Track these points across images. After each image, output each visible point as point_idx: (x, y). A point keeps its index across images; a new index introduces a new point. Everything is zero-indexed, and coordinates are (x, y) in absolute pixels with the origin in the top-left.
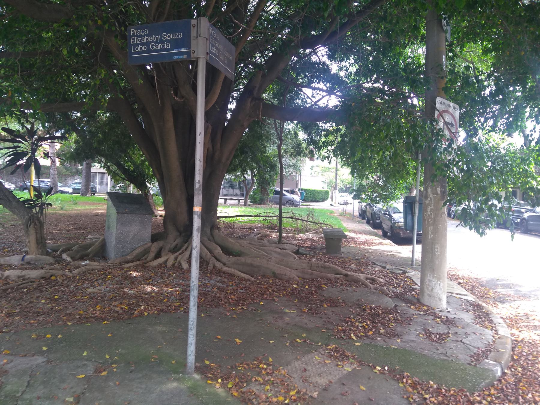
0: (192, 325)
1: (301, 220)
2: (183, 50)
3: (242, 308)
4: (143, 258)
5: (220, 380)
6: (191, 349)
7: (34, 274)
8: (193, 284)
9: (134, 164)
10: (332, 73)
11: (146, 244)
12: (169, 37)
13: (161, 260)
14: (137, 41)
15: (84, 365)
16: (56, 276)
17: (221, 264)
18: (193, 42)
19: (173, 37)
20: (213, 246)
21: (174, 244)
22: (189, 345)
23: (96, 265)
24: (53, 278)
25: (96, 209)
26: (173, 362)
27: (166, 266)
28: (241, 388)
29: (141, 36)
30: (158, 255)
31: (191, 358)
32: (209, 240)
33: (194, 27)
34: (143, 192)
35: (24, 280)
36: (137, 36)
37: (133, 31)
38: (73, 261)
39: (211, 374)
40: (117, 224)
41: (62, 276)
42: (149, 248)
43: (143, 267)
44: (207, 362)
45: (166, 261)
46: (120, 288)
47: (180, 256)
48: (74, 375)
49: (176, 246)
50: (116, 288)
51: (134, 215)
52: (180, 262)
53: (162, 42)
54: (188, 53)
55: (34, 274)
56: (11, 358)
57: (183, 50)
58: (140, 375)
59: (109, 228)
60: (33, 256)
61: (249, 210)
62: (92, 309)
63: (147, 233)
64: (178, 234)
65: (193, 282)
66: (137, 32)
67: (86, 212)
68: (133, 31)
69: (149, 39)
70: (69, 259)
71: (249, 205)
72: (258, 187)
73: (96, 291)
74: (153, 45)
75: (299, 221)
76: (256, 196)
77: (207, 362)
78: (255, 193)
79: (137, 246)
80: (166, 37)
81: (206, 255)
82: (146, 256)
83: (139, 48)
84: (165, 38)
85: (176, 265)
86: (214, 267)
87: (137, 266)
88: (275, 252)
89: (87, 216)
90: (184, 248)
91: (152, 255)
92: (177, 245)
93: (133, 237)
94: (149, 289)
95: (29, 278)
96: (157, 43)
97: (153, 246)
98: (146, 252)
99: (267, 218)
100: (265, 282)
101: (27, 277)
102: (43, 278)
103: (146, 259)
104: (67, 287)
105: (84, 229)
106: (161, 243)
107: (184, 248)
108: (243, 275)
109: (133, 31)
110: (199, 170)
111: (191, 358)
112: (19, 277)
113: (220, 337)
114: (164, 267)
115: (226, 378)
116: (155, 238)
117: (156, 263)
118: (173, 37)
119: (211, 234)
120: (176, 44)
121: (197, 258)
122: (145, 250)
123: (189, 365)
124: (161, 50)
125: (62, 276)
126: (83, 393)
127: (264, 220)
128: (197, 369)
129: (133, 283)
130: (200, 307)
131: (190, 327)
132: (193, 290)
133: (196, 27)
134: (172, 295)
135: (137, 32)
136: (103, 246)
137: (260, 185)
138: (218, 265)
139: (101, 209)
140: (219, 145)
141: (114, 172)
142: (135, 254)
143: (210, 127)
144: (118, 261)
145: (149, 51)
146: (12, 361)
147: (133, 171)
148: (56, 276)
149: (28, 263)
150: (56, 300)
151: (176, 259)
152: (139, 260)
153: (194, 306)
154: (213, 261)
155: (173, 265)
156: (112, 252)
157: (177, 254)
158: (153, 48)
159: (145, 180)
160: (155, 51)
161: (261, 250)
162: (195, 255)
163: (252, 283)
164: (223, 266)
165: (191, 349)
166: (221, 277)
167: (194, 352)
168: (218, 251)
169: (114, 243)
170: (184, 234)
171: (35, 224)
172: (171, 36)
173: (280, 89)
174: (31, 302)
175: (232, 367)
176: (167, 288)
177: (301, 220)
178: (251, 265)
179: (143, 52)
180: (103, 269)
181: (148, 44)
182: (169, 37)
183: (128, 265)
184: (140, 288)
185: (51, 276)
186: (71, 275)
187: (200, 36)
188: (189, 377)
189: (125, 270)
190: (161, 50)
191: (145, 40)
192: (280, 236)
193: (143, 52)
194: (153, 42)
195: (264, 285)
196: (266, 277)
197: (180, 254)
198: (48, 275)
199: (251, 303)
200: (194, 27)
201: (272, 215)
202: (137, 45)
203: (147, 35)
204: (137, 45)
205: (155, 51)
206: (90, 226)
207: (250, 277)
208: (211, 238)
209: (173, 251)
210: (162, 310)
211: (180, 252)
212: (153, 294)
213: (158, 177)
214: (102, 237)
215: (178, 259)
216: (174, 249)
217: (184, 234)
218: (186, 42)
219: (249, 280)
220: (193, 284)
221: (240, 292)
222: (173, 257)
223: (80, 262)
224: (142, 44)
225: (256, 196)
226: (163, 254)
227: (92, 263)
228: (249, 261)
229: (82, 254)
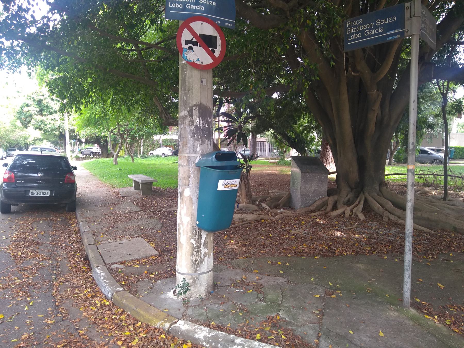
0: (408, 266)
1: (460, 177)
2: (396, 31)
3: (432, 257)
4: (322, 209)
5: (436, 317)
6: (407, 286)
7: (250, 217)
8: (409, 231)
9: (295, 133)
10: (183, 21)
11: (324, 198)
12: (382, 22)
13: (339, 211)
14: (352, 31)
15: (316, 288)
16: (265, 220)
17: (396, 217)
18: (407, 23)
19: (386, 21)
20: (384, 201)
21: (347, 199)
22: (405, 283)
23: (289, 212)
24: (263, 221)
25: (265, 170)
26: (387, 295)
27: (344, 216)
28: (460, 326)
29: (356, 26)
30: (335, 208)
31: (407, 294)
32: (378, 195)
33: (407, 9)
34: (303, 155)
35: (243, 221)
36: (352, 26)
37: (348, 23)
38: (271, 209)
39: (426, 310)
40: (301, 181)
41: (268, 219)
42: (327, 201)
43: (325, 216)
44: (418, 300)
45: (344, 212)
46: (315, 232)
47: (355, 209)
48: (312, 295)
49: (349, 200)
50: (312, 232)
51: (314, 174)
52: (355, 214)
53: (376, 27)
54: (402, 33)
55: (250, 217)
56: (261, 276)
57: (396, 31)
58: (363, 302)
59: (294, 184)
60: (244, 205)
61: (396, 169)
62: (301, 246)
63: (325, 188)
64: (350, 190)
65: (408, 230)
66: (352, 24)
67: (258, 172)
68: (348, 23)
69: (364, 27)
70: (268, 208)
71: (394, 165)
72: (402, 147)
73: (298, 233)
74: (367, 31)
75: (457, 179)
76: (400, 156)
77: (418, 300)
78: (399, 153)
79: (317, 199)
80: (379, 22)
81: (379, 208)
82: (324, 207)
83: (354, 36)
84: (379, 24)
85: (353, 216)
86: (389, 219)
87: (320, 215)
88: (448, 208)
89: (261, 175)
90: (357, 202)
91: (330, 207)
92: (349, 199)
93: (314, 192)
94: (338, 234)
95: (247, 220)
96: (371, 29)
97: (330, 199)
98: (325, 204)
99: (422, 176)
100: (447, 235)
101: (245, 219)
102: (256, 221)
103: (325, 210)
104: (275, 228)
105: (264, 185)
106: (336, 197)
107: (357, 202)
108: (422, 228)
109: (348, 23)
110: (413, 133)
111: (407, 294)
112: (240, 219)
113: (421, 280)
114: (343, 217)
115: (442, 316)
116: (330, 193)
117: (335, 213)
118: (386, 21)
119: (380, 191)
120: (389, 27)
121: (411, 209)
122: (323, 202)
123: (405, 299)
124: (375, 34)
125: (268, 219)
126: (324, 309)
127: (419, 178)
128: (414, 305)
129: (324, 228)
130: (415, 251)
131: (406, 268)
132: (408, 237)
133: (409, 10)
134: (361, 241)
135: (352, 24)
136: (290, 198)
137: (404, 145)
138: (392, 217)
139: (269, 170)
140: (387, 110)
141: (280, 140)
142: (315, 206)
143: (381, 94)
144: (304, 210)
145: (363, 37)
146: (262, 278)
147: (295, 139)
148: (265, 220)
149: (241, 209)
150: (271, 237)
151: (352, 211)
152: (319, 210)
153: (410, 250)
154: (386, 214)
155: (351, 216)
156: (297, 203)
157: (352, 206)
158: (367, 34)
159: (304, 145)
160: (370, 36)
161: (433, 205)
162: (410, 207)
163: (433, 235)
164: (398, 219)
165: (407, 286)
166: (399, 228)
167: (410, 289)
168: (390, 205)
169: (299, 196)
170: (355, 190)
171: (245, 181)
172: (384, 21)
173: (139, 39)
174: (255, 238)
175: (444, 307)
176: (354, 234)
177: (460, 177)
178: (428, 219)
179: (358, 39)
180: (296, 216)
181: (362, 32)
182: (382, 22)
183: (314, 214)
184: (331, 233)
185: (261, 219)
186: (275, 219)
187: (414, 16)
188: (406, 310)
189: (312, 217)
190: (375, 34)
191: (360, 29)
192: (446, 193)
193: (358, 39)
194: (367, 29)
195: (446, 238)
196: (446, 232)
197: (355, 207)
198: (259, 219)
199: (440, 254)
200: (407, 9)
201: (426, 173)
202: (353, 34)
203: (361, 24)
204: (353, 34)
205: (370, 36)
206: (267, 183)
207: (429, 230)
208: (380, 194)
209: (348, 203)
210: (358, 252)
211: (354, 205)
212: (344, 239)
213: (331, 142)
214: (288, 193)
215: (354, 211)
216: (347, 202)
217: (355, 190)
218: (400, 23)
219: (429, 233)
220: (409, 231)
221: (424, 243)
222: (349, 209)
223: (277, 210)
224: (357, 33)
225: (400, 156)
226: (339, 206)
227: (285, 211)
228: (426, 216)
229: (275, 204)
